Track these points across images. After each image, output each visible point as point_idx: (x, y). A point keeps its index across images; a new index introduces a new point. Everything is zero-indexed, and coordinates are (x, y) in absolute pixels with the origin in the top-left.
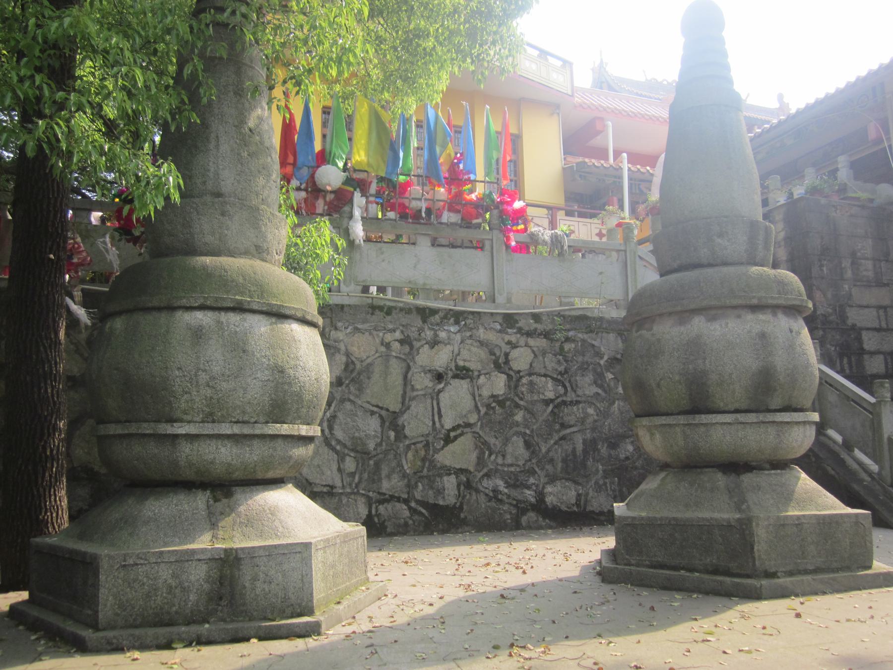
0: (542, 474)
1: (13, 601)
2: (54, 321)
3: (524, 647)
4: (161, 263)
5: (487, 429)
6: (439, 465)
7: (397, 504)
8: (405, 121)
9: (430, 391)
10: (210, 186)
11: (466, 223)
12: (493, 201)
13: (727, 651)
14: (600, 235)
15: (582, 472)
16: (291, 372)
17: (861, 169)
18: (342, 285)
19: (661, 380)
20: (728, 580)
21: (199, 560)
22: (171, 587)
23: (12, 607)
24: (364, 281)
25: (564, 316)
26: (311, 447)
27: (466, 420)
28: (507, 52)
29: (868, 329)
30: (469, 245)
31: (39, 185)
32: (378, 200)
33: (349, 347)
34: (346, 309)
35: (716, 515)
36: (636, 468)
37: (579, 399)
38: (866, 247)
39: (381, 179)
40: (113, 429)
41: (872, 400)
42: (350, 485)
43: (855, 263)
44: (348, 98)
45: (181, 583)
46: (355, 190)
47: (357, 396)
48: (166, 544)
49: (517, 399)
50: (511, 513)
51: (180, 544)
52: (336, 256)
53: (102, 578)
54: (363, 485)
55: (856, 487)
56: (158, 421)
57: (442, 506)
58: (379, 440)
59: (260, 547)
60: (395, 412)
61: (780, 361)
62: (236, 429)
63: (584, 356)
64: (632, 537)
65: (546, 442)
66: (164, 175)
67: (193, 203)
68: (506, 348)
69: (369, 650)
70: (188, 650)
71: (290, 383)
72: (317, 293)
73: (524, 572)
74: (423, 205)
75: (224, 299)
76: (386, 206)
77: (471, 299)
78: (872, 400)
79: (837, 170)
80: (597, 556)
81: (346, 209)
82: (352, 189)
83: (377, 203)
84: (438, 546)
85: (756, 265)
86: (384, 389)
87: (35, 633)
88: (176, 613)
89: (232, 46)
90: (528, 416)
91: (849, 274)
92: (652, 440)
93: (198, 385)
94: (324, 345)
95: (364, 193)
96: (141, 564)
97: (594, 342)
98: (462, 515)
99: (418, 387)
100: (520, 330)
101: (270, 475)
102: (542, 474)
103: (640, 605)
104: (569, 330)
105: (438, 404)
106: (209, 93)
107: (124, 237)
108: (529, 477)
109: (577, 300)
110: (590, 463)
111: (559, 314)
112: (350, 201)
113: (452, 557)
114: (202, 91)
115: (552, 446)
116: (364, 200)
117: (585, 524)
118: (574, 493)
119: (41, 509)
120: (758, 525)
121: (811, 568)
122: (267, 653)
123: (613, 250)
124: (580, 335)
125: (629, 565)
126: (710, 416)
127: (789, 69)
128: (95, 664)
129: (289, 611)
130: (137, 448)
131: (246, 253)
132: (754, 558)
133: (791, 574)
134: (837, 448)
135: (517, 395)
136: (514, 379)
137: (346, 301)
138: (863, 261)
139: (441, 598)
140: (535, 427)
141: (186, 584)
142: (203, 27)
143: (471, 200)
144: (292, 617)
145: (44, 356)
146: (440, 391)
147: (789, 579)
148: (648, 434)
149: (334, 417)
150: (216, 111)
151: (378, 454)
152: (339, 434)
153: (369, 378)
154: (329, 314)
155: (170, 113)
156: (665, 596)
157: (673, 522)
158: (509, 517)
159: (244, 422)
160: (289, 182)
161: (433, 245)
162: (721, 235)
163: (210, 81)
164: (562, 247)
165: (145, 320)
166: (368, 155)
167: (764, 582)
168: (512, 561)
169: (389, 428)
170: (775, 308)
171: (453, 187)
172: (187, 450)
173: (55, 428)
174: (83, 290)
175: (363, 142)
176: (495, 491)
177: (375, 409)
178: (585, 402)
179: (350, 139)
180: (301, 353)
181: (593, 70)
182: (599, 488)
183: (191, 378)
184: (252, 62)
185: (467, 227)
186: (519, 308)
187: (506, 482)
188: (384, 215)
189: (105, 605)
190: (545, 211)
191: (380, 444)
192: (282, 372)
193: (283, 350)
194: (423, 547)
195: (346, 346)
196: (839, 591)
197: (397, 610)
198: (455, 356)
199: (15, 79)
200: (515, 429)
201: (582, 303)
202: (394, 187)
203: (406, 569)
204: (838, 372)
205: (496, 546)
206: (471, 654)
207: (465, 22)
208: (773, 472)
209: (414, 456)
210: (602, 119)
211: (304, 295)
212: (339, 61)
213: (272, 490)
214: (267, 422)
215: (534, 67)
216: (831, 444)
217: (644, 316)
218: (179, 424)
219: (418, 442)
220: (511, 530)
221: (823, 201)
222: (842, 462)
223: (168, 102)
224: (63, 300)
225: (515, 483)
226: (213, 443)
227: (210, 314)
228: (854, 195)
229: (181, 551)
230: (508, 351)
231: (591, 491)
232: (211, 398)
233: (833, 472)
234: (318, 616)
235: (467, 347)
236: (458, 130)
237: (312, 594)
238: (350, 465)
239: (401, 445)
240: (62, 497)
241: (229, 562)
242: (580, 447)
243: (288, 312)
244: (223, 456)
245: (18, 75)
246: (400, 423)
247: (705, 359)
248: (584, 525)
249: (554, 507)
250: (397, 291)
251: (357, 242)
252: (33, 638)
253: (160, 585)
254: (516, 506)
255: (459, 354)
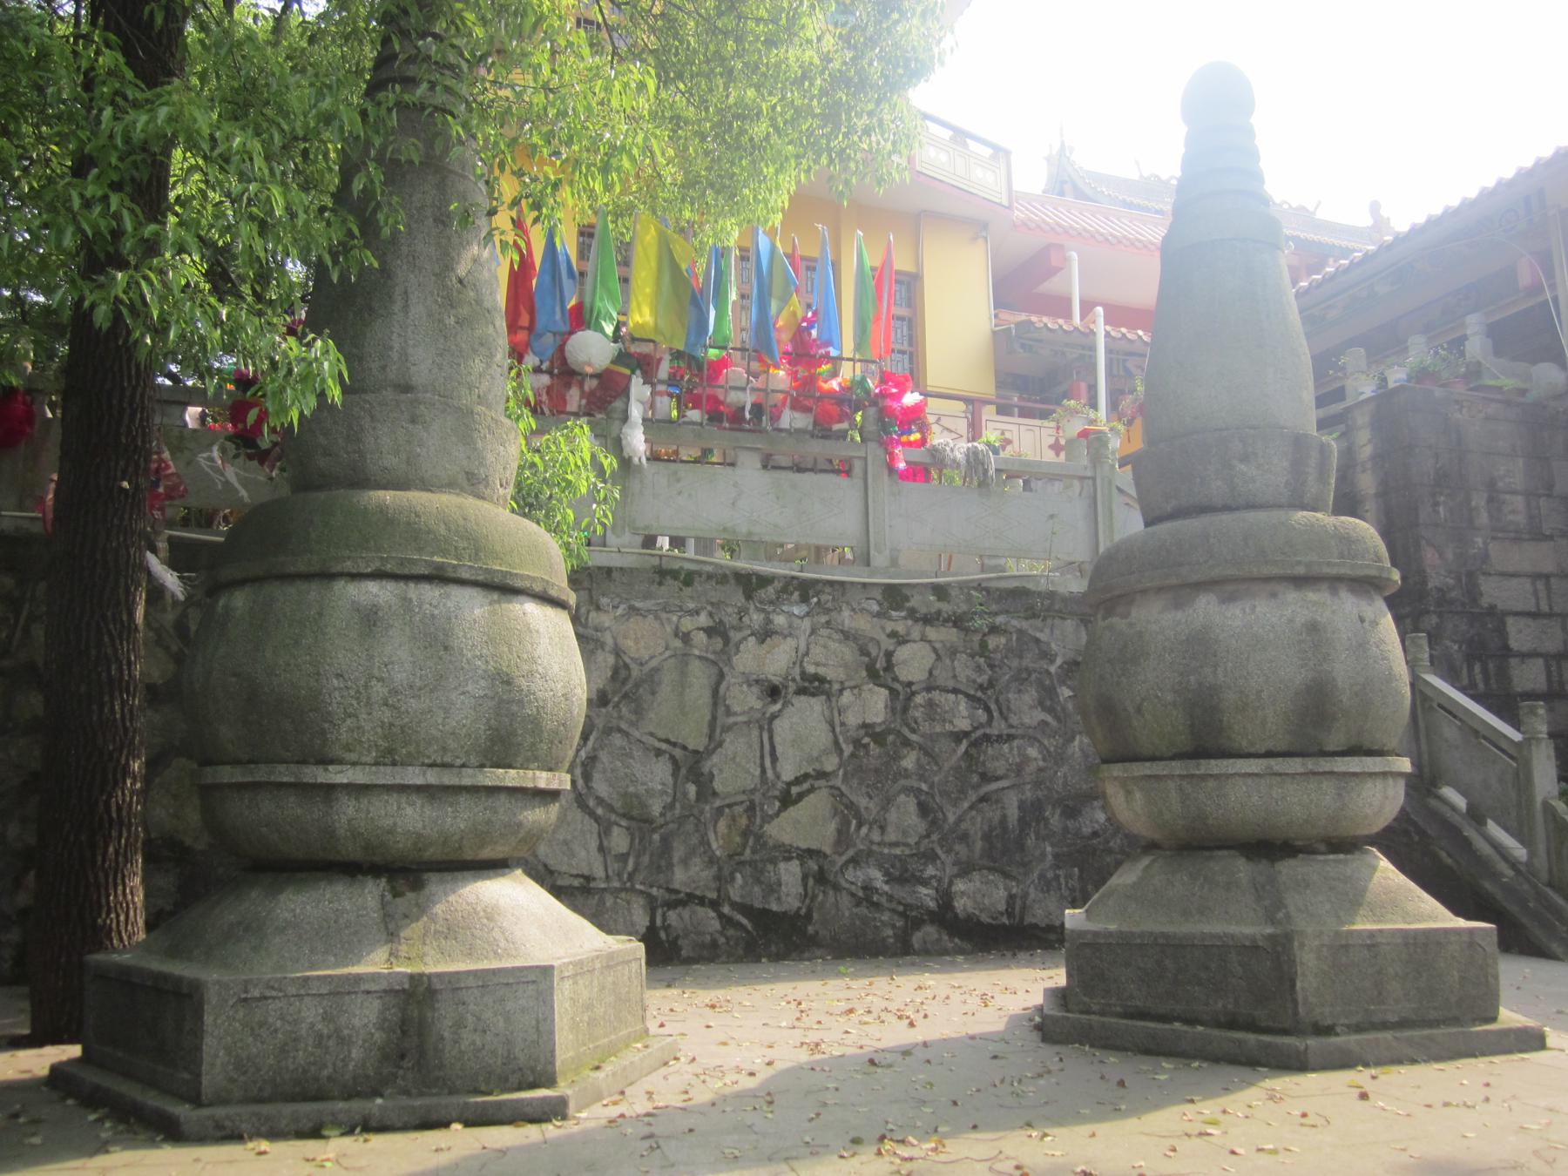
0: (948, 859)
1: (55, 1060)
2: (127, 591)
3: (903, 1142)
4: (308, 506)
5: (855, 782)
6: (771, 843)
7: (699, 909)
8: (720, 254)
9: (757, 715)
10: (392, 373)
11: (822, 430)
12: (867, 392)
13: (1238, 1150)
14: (1056, 448)
15: (1017, 857)
16: (523, 683)
17: (1504, 338)
18: (609, 533)
19: (1143, 700)
20: (1251, 1037)
21: (368, 992)
22: (321, 1036)
23: (55, 1069)
24: (646, 527)
25: (987, 590)
26: (554, 809)
27: (817, 766)
28: (889, 146)
29: (1517, 614)
30: (828, 467)
31: (105, 374)
32: (671, 390)
33: (620, 641)
34: (615, 575)
35: (1233, 929)
36: (1110, 851)
37: (1013, 731)
38: (1514, 473)
39: (677, 355)
40: (227, 774)
41: (1516, 736)
42: (619, 875)
43: (1494, 500)
44: (622, 215)
45: (337, 1030)
46: (633, 372)
47: (632, 724)
48: (312, 967)
49: (906, 731)
50: (894, 927)
51: (336, 966)
52: (600, 485)
53: (208, 1019)
54: (640, 877)
55: (1488, 885)
56: (304, 762)
57: (775, 914)
58: (669, 800)
59: (469, 973)
60: (696, 752)
61: (1342, 670)
62: (432, 777)
63: (1021, 657)
64: (1092, 965)
65: (955, 806)
66: (316, 359)
67: (366, 401)
68: (888, 644)
69: (646, 1144)
70: (347, 1141)
71: (520, 702)
72: (567, 546)
73: (912, 1025)
74: (748, 399)
75: (413, 562)
76: (688, 399)
77: (831, 558)
78: (1516, 736)
79: (1464, 338)
80: (1037, 999)
81: (618, 404)
82: (627, 372)
83: (671, 395)
84: (767, 981)
85: (1304, 507)
86: (680, 711)
87: (95, 1111)
88: (329, 1078)
89: (430, 145)
90: (924, 760)
91: (1483, 519)
92: (1128, 802)
93: (368, 704)
94: (579, 636)
95: (648, 379)
96: (274, 998)
97: (1038, 635)
98: (811, 929)
99: (736, 708)
100: (912, 613)
101: (486, 853)
102: (948, 859)
103: (1102, 1078)
104: (996, 614)
105: (771, 738)
106: (392, 220)
107: (242, 451)
108: (925, 864)
109: (1011, 563)
110: (1030, 841)
111: (979, 587)
112: (625, 392)
113: (790, 998)
114: (381, 217)
115: (965, 812)
116: (647, 390)
117: (1030, 948)
118: (1002, 893)
119: (100, 907)
120: (1302, 945)
121: (1393, 1018)
122: (478, 1146)
123: (1073, 477)
124: (1015, 622)
125: (1088, 1012)
126: (1225, 762)
127: (1378, 163)
128: (197, 1160)
129: (514, 1079)
130: (267, 806)
131: (451, 485)
132: (1295, 1002)
133: (1358, 1029)
134: (1456, 820)
135: (908, 725)
136: (901, 698)
137: (615, 561)
138: (1508, 497)
139: (769, 1064)
140: (936, 779)
141: (346, 1032)
142: (383, 112)
143: (832, 391)
144: (520, 1088)
145: (109, 651)
146: (774, 717)
147: (1354, 1037)
148: (1122, 792)
149: (593, 759)
150: (405, 249)
151: (667, 823)
152: (601, 787)
153: (653, 693)
154: (586, 584)
155: (330, 252)
156: (1145, 1063)
157: (1161, 941)
158: (890, 932)
159: (444, 765)
160: (520, 360)
161: (765, 467)
162: (1245, 458)
163: (395, 199)
164: (986, 471)
165: (285, 596)
166: (655, 312)
167: (1312, 1042)
168: (893, 1007)
169: (688, 779)
170: (1335, 582)
171: (799, 368)
172: (351, 811)
173: (126, 771)
174: (170, 540)
175: (648, 290)
176: (868, 888)
177: (664, 746)
178: (1023, 737)
179: (625, 280)
180: (540, 651)
181: (1048, 159)
182: (1046, 885)
183: (358, 692)
184: (463, 168)
185: (823, 437)
186: (910, 575)
187: (887, 873)
188: (681, 415)
189: (213, 1065)
190: (961, 406)
191: (671, 806)
192: (508, 682)
193: (510, 646)
194: (742, 981)
195: (614, 638)
196: (1439, 1058)
197: (694, 1081)
198: (801, 657)
199: (76, 203)
200: (903, 782)
201: (1019, 568)
202: (700, 368)
203: (712, 1018)
204: (1463, 690)
205: (866, 981)
206: (815, 1150)
207: (823, 92)
208: (1331, 857)
209: (729, 827)
210: (1060, 247)
211: (544, 552)
212: (605, 169)
213: (489, 878)
214: (482, 766)
215: (943, 157)
216: (1449, 814)
217: (1117, 593)
218: (338, 768)
219: (736, 804)
220: (894, 955)
221: (1438, 393)
222: (1466, 844)
223: (325, 235)
224: (143, 557)
225: (902, 875)
226: (393, 799)
227: (391, 586)
228: (1492, 383)
229: (340, 977)
230: (891, 648)
231: (1032, 890)
232: (391, 725)
233: (1449, 861)
234: (563, 1089)
235: (822, 641)
236: (811, 265)
237: (553, 1051)
238: (619, 840)
239: (707, 808)
240: (135, 889)
241: (416, 998)
242: (1013, 813)
243: (518, 584)
244: (410, 821)
245: (82, 196)
246: (706, 770)
247: (1215, 666)
248: (1020, 948)
249: (969, 917)
250: (705, 545)
251: (636, 460)
252: (92, 1117)
253: (303, 1032)
254: (903, 915)
255: (807, 654)
